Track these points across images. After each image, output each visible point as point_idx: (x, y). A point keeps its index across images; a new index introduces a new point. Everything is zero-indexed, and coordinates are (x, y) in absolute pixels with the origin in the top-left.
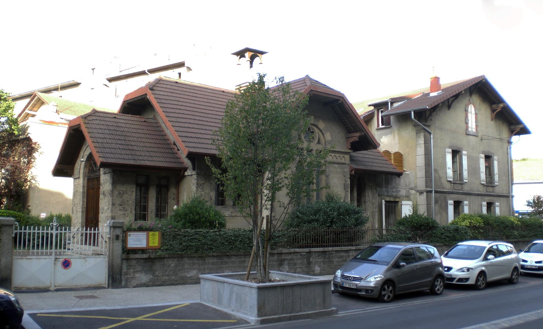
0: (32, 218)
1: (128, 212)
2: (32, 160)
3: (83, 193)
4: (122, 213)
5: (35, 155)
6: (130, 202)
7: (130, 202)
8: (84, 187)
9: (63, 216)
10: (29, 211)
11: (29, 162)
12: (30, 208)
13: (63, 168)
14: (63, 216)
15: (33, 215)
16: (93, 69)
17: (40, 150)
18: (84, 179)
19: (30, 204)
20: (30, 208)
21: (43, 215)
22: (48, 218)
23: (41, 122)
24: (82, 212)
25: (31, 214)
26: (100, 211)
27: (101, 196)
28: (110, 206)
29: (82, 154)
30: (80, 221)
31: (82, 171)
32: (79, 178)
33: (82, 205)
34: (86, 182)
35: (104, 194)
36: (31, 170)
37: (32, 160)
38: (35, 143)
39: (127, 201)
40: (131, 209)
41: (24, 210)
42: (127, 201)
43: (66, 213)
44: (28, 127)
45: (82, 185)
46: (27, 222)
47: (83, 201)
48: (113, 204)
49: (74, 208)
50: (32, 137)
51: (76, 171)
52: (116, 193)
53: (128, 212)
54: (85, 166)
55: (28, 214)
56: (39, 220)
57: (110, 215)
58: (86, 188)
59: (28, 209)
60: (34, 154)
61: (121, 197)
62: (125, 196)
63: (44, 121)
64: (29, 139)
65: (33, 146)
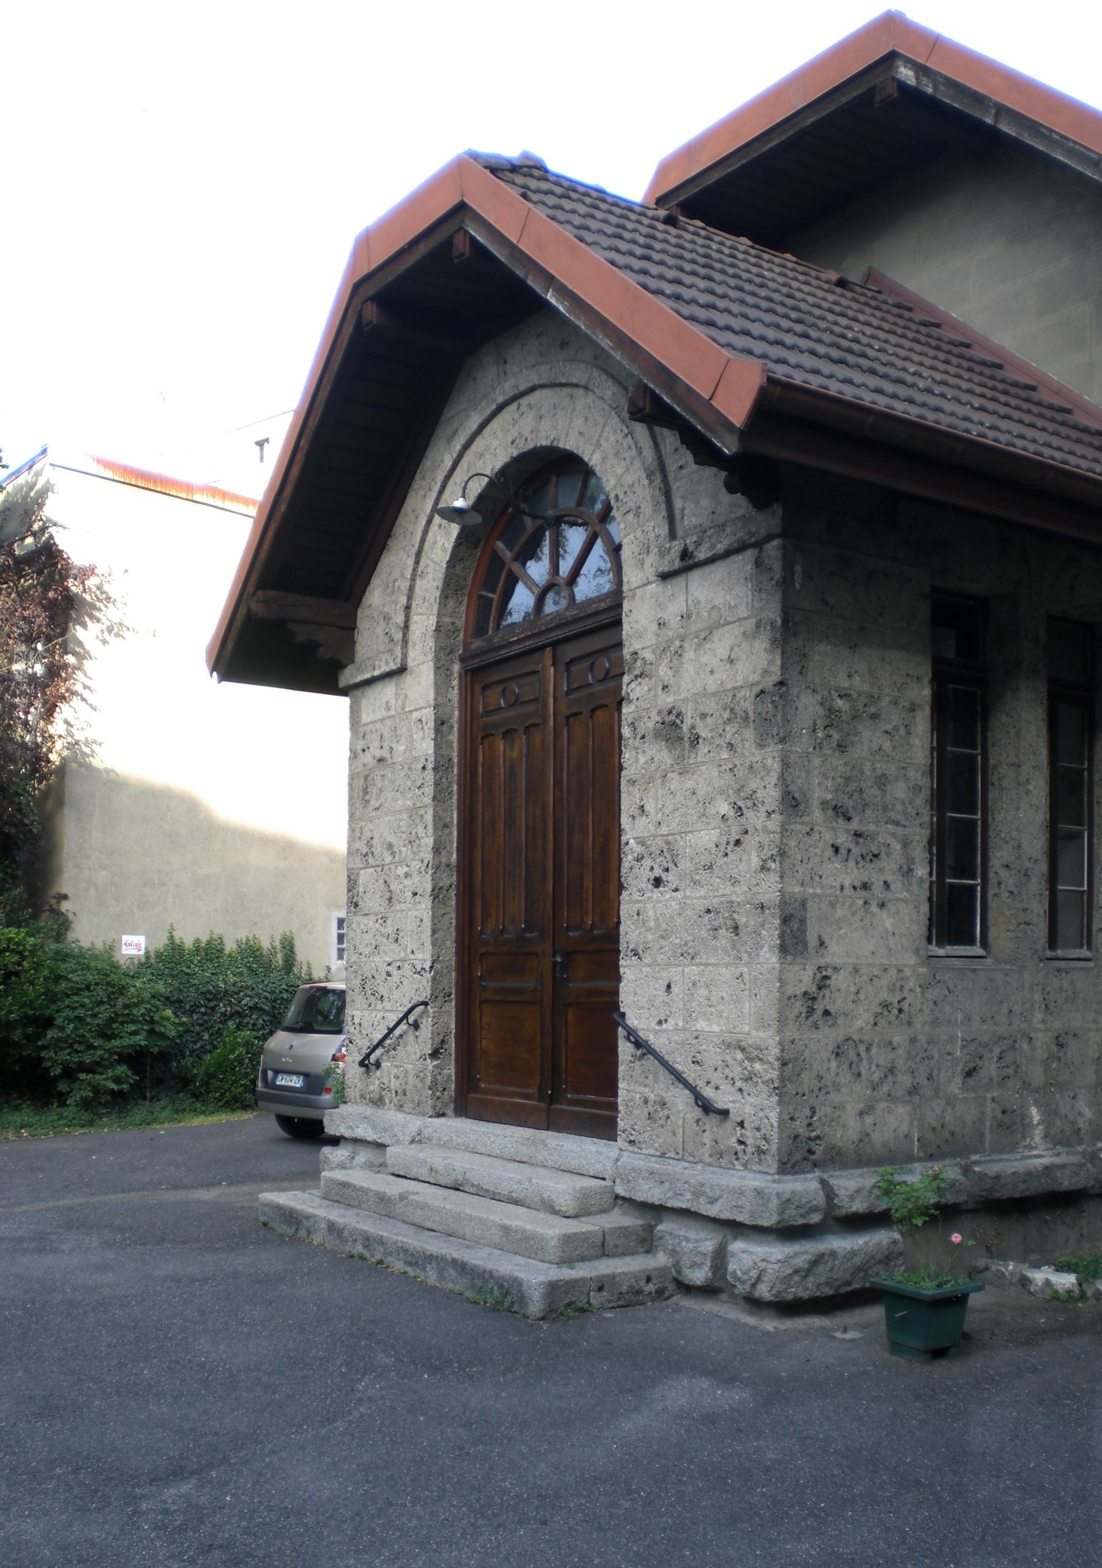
0: (82, 959)
1: (889, 869)
2: (70, 659)
3: (441, 766)
4: (851, 875)
5: (86, 634)
6: (899, 791)
7: (899, 791)
8: (441, 723)
9: (230, 946)
10: (63, 924)
11: (55, 671)
12: (65, 906)
13: (289, 622)
14: (230, 946)
15: (85, 943)
16: (260, 444)
17: (109, 614)
18: (441, 670)
19: (65, 886)
20: (65, 906)
21: (133, 946)
22: (159, 955)
23: (109, 474)
24: (437, 894)
25: (71, 936)
26: (635, 876)
27: (639, 759)
28: (763, 823)
29: (440, 457)
30: (424, 957)
31: (424, 622)
32: (402, 670)
33: (437, 850)
34: (454, 694)
35: (672, 730)
36: (64, 712)
37: (70, 659)
38: (85, 573)
39: (882, 780)
40: (905, 844)
41: (36, 916)
42: (882, 780)
43: (242, 934)
44: (43, 494)
45: (428, 714)
46: (58, 978)
47: (440, 824)
48: (792, 803)
49: (365, 876)
50: (63, 541)
51: (372, 645)
52: (808, 707)
53: (889, 869)
54: (451, 586)
55: (59, 937)
56: (115, 966)
57: (769, 889)
58: (454, 737)
59: (56, 913)
60: (79, 632)
61: (842, 748)
62: (869, 739)
63: (127, 470)
64: (48, 559)
65: (73, 586)
